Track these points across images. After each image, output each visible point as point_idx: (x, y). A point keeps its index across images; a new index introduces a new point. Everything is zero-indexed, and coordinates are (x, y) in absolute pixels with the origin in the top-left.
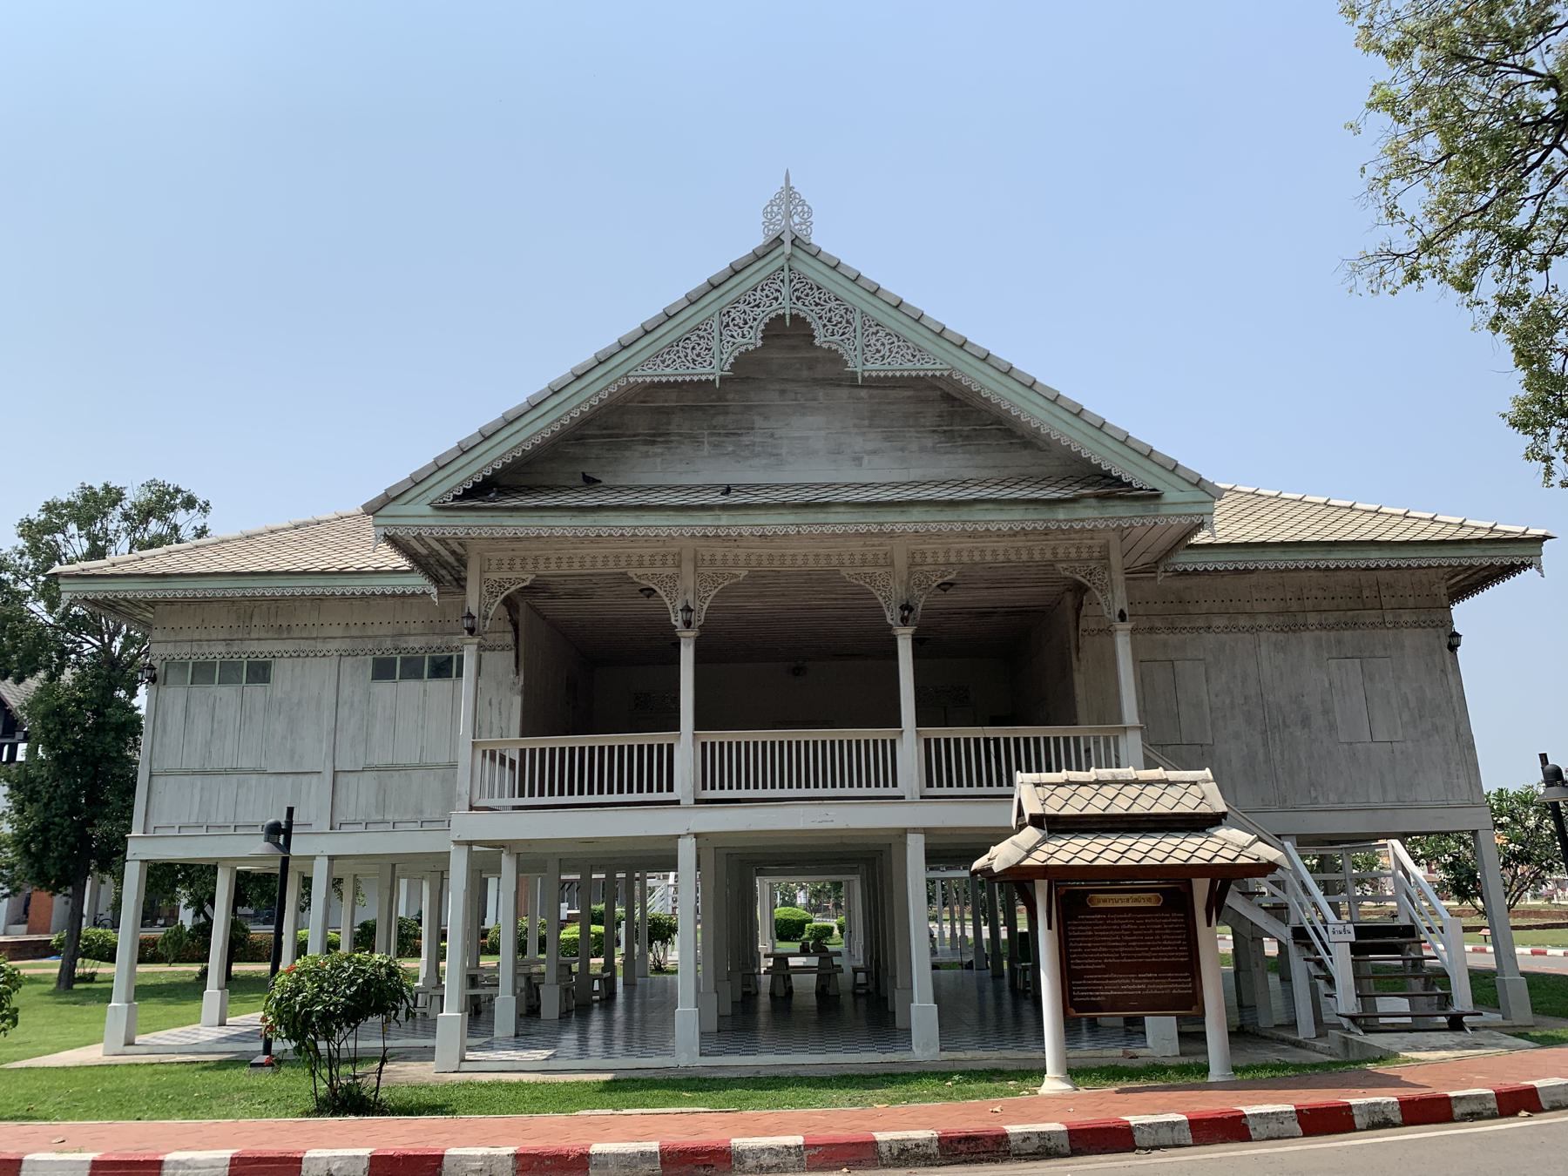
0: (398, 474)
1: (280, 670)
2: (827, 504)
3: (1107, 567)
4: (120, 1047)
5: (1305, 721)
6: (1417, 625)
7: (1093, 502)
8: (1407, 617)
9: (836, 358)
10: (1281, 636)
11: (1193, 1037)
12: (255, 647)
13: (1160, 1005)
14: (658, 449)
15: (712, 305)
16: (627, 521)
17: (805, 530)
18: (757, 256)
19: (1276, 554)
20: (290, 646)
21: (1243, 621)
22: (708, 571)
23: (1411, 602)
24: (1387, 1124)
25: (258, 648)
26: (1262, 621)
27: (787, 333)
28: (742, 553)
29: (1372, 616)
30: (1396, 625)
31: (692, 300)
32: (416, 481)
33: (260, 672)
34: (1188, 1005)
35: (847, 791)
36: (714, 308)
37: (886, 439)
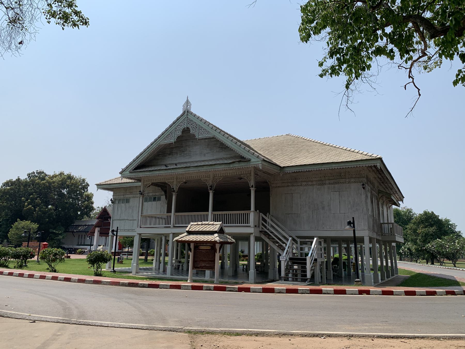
0: (124, 167)
1: (131, 200)
2: (189, 167)
3: (251, 175)
4: (108, 268)
5: (323, 208)
6: (355, 182)
7: (237, 163)
8: (353, 180)
9: (194, 136)
10: (319, 186)
11: (213, 275)
12: (127, 196)
13: (208, 268)
14: (170, 156)
15: (173, 128)
16: (157, 172)
17: (186, 172)
18: (182, 115)
19: (309, 167)
20: (132, 196)
21: (310, 183)
22: (179, 180)
23: (354, 176)
24: (210, 290)
26: (314, 183)
27: (186, 131)
28: (185, 176)
30: (349, 182)
31: (171, 126)
32: (127, 167)
33: (128, 201)
34: (212, 268)
35: (231, 225)
36: (174, 128)
37: (211, 150)
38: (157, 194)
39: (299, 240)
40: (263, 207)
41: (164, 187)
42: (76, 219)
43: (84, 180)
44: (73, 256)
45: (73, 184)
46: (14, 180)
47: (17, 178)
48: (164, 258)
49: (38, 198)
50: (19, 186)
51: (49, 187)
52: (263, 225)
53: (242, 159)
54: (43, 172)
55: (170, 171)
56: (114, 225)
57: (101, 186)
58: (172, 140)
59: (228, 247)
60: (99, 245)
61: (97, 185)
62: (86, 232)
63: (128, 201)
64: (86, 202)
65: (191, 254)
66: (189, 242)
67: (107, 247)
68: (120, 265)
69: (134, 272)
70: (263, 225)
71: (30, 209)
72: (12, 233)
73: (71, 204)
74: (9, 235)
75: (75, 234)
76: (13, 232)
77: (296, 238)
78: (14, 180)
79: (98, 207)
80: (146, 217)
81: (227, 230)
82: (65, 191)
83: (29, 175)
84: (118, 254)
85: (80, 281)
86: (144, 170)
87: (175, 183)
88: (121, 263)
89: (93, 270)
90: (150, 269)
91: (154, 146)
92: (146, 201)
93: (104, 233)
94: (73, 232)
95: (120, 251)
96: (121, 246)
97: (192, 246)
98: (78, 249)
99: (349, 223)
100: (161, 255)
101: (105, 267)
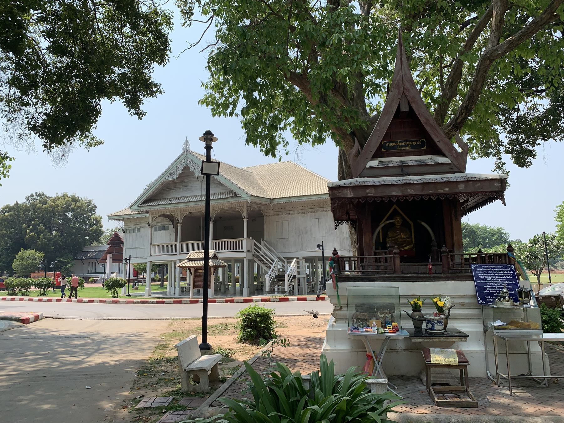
0: (132, 201)
1: (141, 229)
5: (306, 233)
12: (137, 226)
15: (175, 166)
18: (182, 155)
21: (296, 212)
25: (138, 226)
26: (300, 211)
27: (186, 168)
29: (321, 209)
38: (165, 223)
39: (286, 261)
40: (257, 233)
41: (171, 218)
42: (85, 245)
43: (90, 202)
44: (86, 285)
45: (78, 207)
46: (12, 205)
47: (15, 203)
48: (179, 283)
49: (41, 224)
50: (19, 212)
51: (53, 212)
52: (255, 249)
53: (235, 195)
54: (43, 195)
55: (173, 206)
56: (126, 254)
57: (111, 217)
58: (175, 177)
59: (220, 270)
60: (112, 271)
61: (109, 216)
62: (96, 259)
63: (138, 230)
64: (95, 226)
65: (192, 277)
66: (189, 268)
67: (121, 274)
68: (134, 291)
69: (147, 295)
70: (255, 249)
71: (32, 236)
72: (16, 264)
73: (78, 229)
74: (13, 266)
75: (85, 261)
76: (17, 263)
77: (284, 259)
78: (12, 205)
79: (108, 230)
80: (157, 246)
81: (220, 256)
82: (70, 215)
83: (27, 198)
84: (133, 282)
85: (101, 302)
86: (150, 204)
87: (179, 215)
88: (137, 289)
89: (110, 294)
90: (165, 293)
91: (159, 182)
92: (155, 230)
93: (117, 259)
94: (82, 259)
95: (135, 278)
96: (136, 273)
97: (192, 270)
98: (89, 278)
99: (318, 246)
100: (175, 280)
101: (122, 291)
